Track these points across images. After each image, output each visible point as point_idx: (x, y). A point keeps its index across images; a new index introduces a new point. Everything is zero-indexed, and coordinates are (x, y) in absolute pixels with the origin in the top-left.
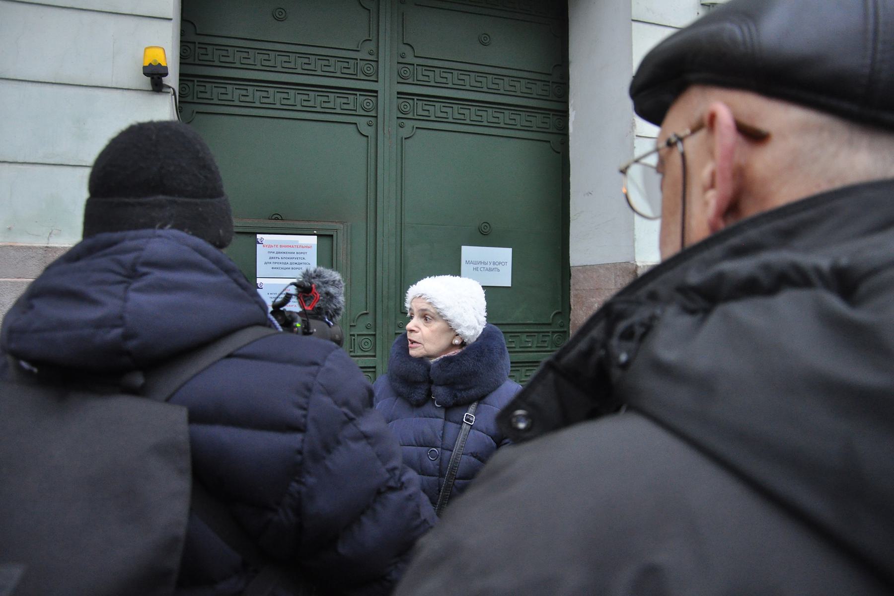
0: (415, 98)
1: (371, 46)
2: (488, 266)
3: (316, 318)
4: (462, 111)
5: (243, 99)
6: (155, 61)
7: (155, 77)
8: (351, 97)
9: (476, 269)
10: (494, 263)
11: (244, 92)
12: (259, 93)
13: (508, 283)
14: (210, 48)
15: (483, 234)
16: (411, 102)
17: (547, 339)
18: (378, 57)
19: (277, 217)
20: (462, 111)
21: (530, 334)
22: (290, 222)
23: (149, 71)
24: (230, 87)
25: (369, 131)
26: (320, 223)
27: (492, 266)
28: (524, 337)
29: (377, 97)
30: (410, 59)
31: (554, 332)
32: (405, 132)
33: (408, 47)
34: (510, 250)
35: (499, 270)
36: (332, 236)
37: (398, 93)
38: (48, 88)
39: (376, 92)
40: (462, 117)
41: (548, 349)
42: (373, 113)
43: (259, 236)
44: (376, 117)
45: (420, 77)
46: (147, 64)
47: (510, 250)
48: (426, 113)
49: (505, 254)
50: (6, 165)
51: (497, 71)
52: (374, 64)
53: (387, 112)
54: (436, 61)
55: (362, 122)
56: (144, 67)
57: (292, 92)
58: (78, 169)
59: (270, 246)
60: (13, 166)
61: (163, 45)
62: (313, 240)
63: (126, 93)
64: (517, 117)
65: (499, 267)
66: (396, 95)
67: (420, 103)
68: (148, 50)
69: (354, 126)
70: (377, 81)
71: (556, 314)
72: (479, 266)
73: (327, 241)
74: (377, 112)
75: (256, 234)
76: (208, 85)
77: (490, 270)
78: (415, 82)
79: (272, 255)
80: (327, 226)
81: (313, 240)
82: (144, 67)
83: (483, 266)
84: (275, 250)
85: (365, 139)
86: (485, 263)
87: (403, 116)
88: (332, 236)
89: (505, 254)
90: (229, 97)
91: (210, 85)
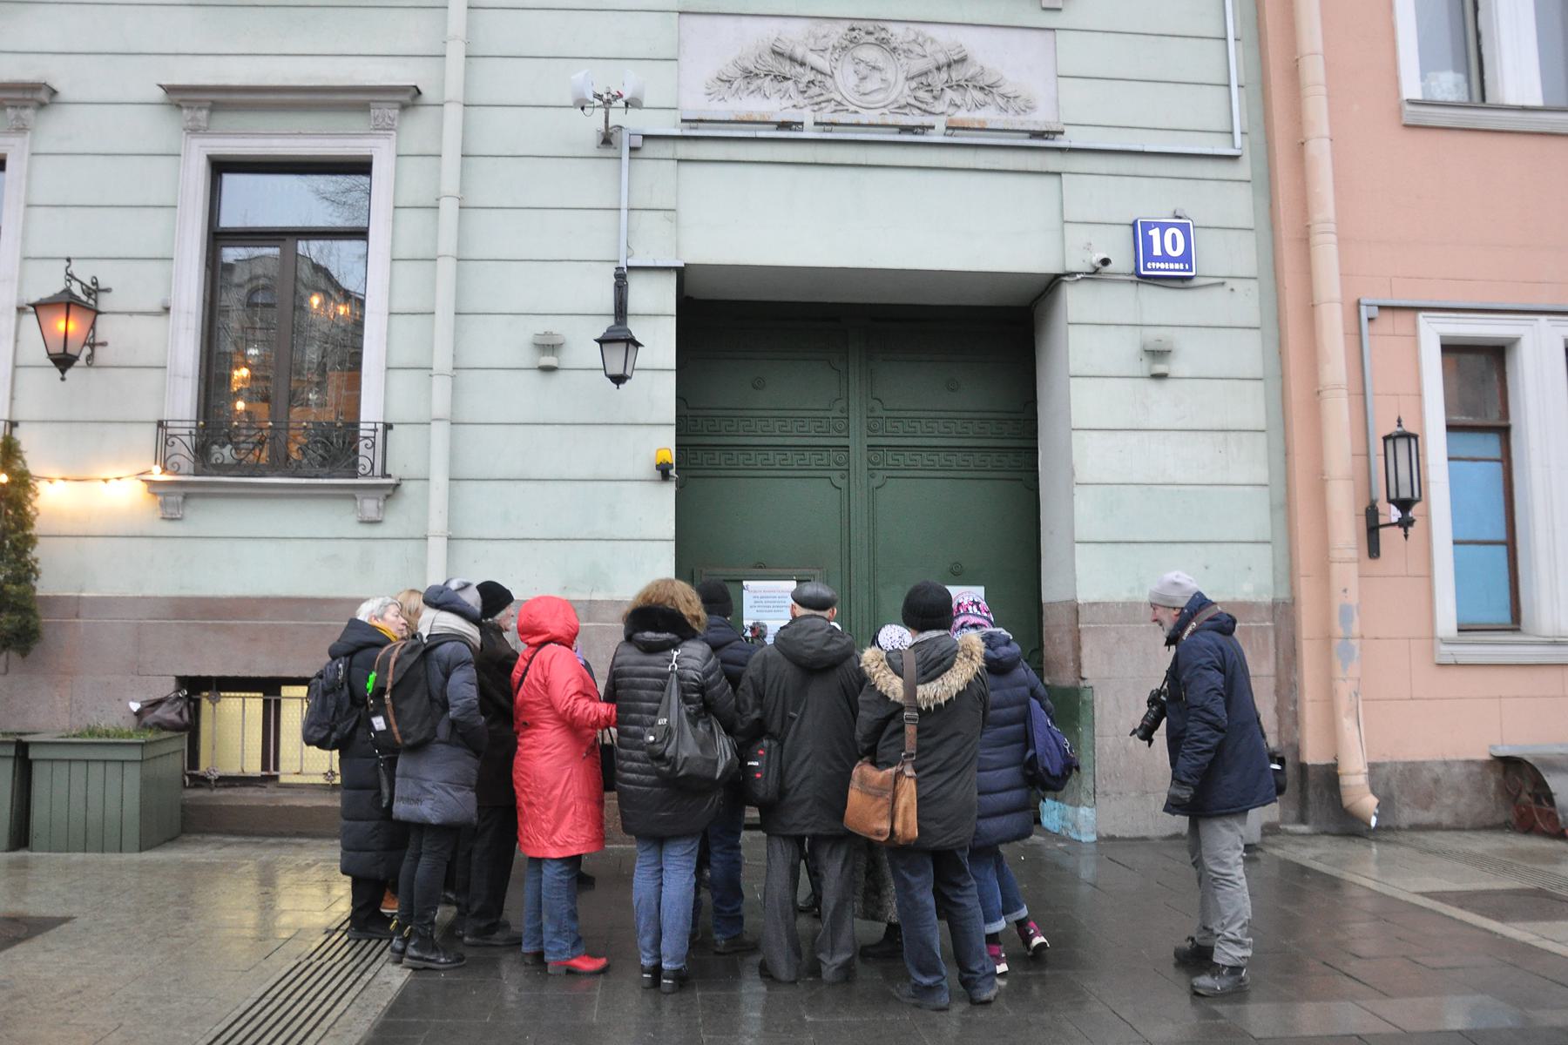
19: (760, 566)
32: (875, 482)
51: (932, 414)
61: (665, 444)
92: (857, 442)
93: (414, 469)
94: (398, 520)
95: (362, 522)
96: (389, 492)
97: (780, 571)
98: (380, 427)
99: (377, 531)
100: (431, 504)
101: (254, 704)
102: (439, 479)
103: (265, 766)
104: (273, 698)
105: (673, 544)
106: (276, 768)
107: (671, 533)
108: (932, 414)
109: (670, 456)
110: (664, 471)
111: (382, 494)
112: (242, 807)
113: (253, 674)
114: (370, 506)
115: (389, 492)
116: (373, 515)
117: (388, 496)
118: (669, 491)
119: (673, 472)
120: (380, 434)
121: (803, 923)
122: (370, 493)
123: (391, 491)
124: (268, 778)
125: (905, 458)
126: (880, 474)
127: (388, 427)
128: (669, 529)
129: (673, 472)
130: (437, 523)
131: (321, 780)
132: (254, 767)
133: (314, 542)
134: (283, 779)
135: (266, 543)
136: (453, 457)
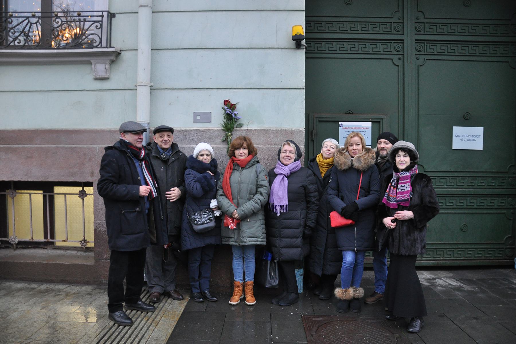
0: (426, 42)
1: (400, 14)
2: (469, 138)
3: (118, 183)
4: (463, 48)
5: (341, 49)
6: (298, 32)
7: (299, 41)
8: (389, 44)
9: (462, 140)
10: (472, 136)
11: (331, 46)
12: (350, 46)
13: (481, 148)
14: (312, 23)
15: (465, 119)
16: (423, 45)
17: (505, 181)
18: (403, 20)
19: (350, 112)
20: (453, 48)
21: (494, 178)
22: (357, 115)
23: (295, 38)
24: (334, 44)
25: (400, 63)
26: (373, 115)
27: (471, 138)
28: (490, 180)
29: (403, 43)
30: (422, 20)
31: (509, 177)
32: (420, 62)
33: (421, 14)
34: (482, 128)
35: (475, 140)
36: (380, 122)
37: (416, 40)
38: (247, 50)
39: (403, 40)
40: (453, 51)
41: (505, 187)
42: (401, 53)
43: (340, 123)
44: (403, 55)
45: (428, 30)
46: (294, 35)
47: (482, 128)
48: (432, 51)
49: (479, 131)
50: (228, 90)
51: (452, 21)
52: (401, 24)
53: (409, 51)
54: (335, 18)
55: (395, 58)
56: (293, 36)
57: (356, 44)
58: (261, 90)
59: (346, 128)
60: (231, 90)
61: (298, 24)
62: (369, 125)
63: (283, 50)
64: (498, 49)
65: (476, 138)
66: (414, 42)
67: (428, 45)
68: (294, 28)
69: (390, 61)
70: (403, 34)
71: (512, 166)
72: (463, 138)
73: (376, 125)
74: (404, 52)
75: (339, 121)
76: (323, 43)
77: (470, 140)
78: (426, 33)
79: (347, 133)
80: (377, 117)
81: (369, 125)
82: (293, 36)
83: (467, 138)
84: (349, 130)
85: (397, 67)
86: (467, 136)
87: (418, 53)
88: (380, 122)
89: (479, 131)
90: (323, 49)
91: (379, 44)
92: (409, 37)
93: (128, 45)
94: (119, 77)
95: (96, 79)
96: (113, 58)
97: (361, 116)
98: (105, 14)
99: (105, 85)
100: (138, 66)
101: (38, 198)
102: (144, 47)
103: (46, 237)
104: (47, 194)
105: (303, 91)
106: (53, 237)
107: (302, 85)
108: (452, 21)
109: (301, 30)
110: (297, 40)
111: (108, 59)
112: (33, 264)
113: (30, 180)
114: (101, 68)
115: (113, 58)
116: (103, 75)
117: (112, 62)
118: (301, 54)
119: (303, 42)
120: (105, 19)
121: (76, 14)
122: (100, 59)
123: (114, 57)
124: (48, 244)
125: (438, 48)
126: (422, 58)
127: (112, 15)
128: (300, 80)
129: (303, 42)
130: (143, 76)
131: (79, 245)
132: (39, 237)
133: (66, 93)
134: (58, 244)
135: (37, 94)
136: (154, 34)
